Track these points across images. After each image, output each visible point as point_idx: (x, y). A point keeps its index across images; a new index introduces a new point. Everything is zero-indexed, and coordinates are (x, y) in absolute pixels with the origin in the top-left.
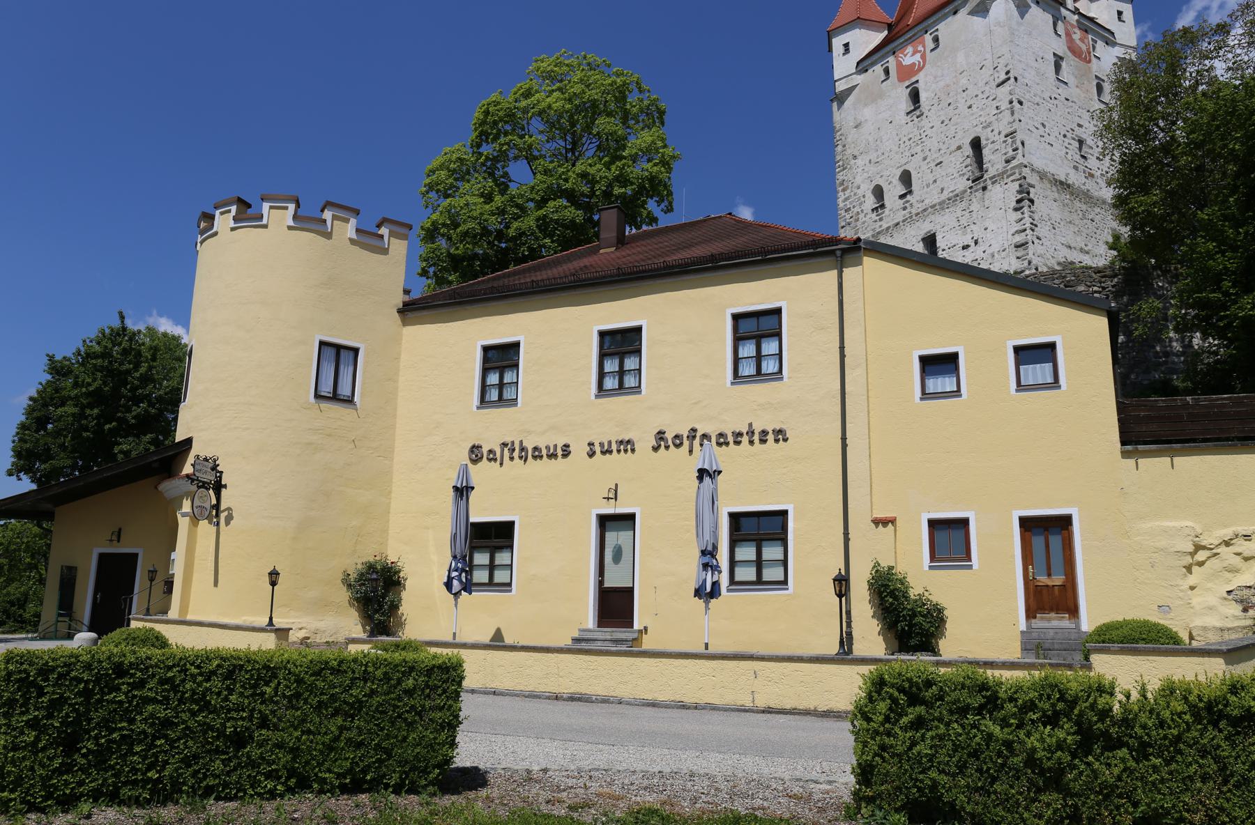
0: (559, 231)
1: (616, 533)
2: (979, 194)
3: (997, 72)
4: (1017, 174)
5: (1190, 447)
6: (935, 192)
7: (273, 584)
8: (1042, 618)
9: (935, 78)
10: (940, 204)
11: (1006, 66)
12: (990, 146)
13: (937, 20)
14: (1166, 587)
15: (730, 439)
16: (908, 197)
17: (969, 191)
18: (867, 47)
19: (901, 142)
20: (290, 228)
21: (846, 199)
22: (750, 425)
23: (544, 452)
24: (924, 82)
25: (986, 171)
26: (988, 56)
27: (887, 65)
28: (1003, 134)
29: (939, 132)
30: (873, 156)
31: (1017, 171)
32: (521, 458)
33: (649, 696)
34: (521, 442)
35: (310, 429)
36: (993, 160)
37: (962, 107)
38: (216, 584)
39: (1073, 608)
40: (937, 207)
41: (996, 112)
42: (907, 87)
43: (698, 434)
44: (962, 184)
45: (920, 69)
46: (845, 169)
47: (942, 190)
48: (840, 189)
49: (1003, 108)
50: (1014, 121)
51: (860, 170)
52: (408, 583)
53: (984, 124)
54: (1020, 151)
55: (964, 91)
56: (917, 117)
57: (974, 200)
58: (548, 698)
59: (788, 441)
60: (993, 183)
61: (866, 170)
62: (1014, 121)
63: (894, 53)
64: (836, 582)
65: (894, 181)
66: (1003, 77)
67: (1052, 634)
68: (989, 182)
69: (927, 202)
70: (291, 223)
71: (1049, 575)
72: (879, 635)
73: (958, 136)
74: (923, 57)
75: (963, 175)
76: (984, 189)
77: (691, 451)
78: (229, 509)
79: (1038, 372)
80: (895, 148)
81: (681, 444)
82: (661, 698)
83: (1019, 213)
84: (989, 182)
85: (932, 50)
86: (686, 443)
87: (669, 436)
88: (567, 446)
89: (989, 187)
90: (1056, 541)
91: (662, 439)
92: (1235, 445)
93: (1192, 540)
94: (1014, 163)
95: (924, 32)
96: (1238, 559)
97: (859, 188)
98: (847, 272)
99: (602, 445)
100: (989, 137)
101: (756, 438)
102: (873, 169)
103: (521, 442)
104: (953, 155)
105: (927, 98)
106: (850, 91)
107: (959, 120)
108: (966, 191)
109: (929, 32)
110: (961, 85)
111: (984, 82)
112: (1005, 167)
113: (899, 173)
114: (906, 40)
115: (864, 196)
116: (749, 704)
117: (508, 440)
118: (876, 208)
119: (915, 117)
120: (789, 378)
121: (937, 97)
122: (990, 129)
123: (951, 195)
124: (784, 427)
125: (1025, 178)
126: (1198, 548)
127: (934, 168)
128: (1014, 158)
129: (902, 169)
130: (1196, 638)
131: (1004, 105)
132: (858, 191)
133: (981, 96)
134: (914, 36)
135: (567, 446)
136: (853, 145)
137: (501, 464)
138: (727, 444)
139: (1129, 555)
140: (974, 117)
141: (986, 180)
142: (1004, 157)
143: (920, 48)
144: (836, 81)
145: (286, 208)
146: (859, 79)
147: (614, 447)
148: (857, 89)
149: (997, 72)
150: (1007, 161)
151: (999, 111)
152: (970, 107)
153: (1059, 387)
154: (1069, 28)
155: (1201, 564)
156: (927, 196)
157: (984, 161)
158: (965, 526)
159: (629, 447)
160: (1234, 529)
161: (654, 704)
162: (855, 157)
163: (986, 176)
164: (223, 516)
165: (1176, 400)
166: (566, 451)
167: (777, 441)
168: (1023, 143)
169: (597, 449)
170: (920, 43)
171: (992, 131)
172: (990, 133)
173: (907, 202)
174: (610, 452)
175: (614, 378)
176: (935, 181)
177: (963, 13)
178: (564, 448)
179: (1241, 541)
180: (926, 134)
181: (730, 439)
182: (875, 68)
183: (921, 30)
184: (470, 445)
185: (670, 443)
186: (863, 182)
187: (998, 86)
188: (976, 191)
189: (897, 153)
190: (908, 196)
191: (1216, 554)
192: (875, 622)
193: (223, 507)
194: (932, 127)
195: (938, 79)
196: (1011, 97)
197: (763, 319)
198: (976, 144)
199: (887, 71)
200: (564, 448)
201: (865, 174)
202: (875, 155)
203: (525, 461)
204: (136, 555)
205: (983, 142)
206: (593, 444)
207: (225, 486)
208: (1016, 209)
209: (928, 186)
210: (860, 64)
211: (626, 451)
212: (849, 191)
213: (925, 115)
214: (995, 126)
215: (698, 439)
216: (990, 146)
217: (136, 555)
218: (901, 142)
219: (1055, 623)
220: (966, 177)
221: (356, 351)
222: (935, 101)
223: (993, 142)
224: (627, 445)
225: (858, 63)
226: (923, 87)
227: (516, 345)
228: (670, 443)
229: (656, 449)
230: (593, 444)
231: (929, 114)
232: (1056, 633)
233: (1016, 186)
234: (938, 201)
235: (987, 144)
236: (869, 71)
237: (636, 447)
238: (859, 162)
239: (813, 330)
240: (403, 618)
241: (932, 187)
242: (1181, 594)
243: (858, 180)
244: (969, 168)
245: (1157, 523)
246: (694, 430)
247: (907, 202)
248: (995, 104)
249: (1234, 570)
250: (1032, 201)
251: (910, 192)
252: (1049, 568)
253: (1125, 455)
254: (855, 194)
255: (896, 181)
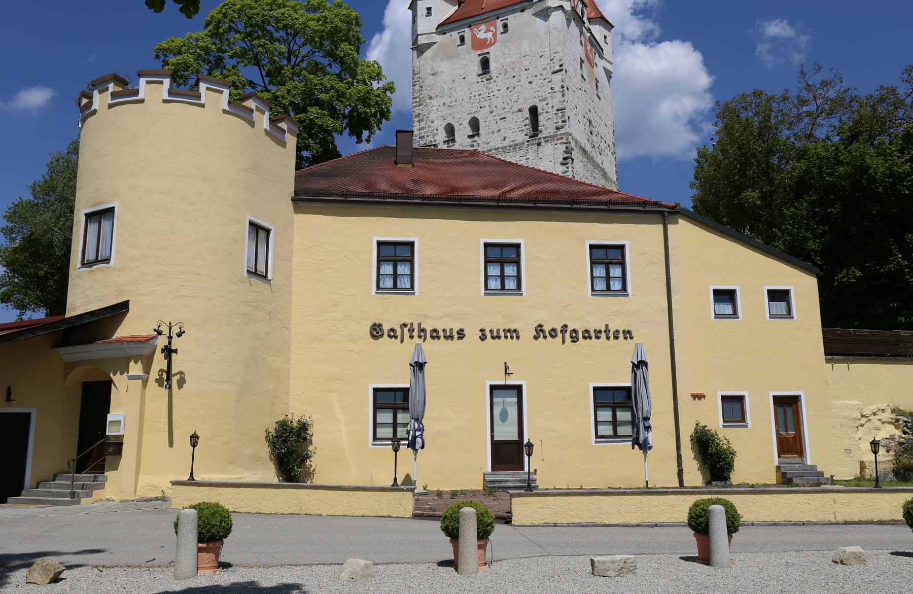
0: (322, 135)
1: (502, 399)
2: (535, 147)
3: (553, 63)
4: (565, 139)
5: (857, 358)
6: (499, 139)
7: (194, 445)
8: (784, 457)
9: (503, 54)
10: (503, 148)
11: (560, 61)
12: (544, 115)
13: (508, 12)
14: (848, 438)
15: (593, 334)
16: (476, 138)
17: (526, 143)
18: (444, 15)
19: (472, 95)
20: (225, 111)
21: (420, 129)
22: (607, 326)
23: (441, 334)
24: (494, 54)
25: (541, 132)
26: (547, 49)
27: (463, 33)
28: (555, 108)
29: (504, 95)
30: (447, 101)
31: (565, 137)
32: (420, 337)
33: (768, 519)
34: (419, 324)
35: (245, 301)
36: (547, 125)
37: (524, 81)
38: (171, 444)
39: (799, 450)
40: (500, 150)
41: (551, 91)
42: (479, 55)
43: (569, 329)
44: (521, 137)
45: (491, 44)
46: (422, 105)
47: (505, 138)
48: (416, 120)
49: (556, 90)
50: (564, 101)
51: (434, 109)
52: (313, 439)
53: (541, 98)
54: (567, 123)
55: (526, 70)
56: (487, 80)
57: (530, 151)
58: (842, 524)
59: (634, 339)
60: (546, 142)
61: (440, 110)
62: (564, 101)
63: (470, 26)
64: (872, 445)
65: (464, 123)
66: (557, 68)
67: (797, 467)
68: (543, 140)
69: (491, 144)
70: (226, 108)
71: (787, 431)
72: (698, 470)
73: (521, 101)
74: (495, 35)
75: (523, 131)
76: (539, 144)
77: (564, 342)
78: (181, 373)
79: (780, 307)
80: (467, 99)
81: (556, 336)
82: (777, 520)
83: (564, 167)
84: (543, 140)
85: (502, 33)
86: (560, 335)
87: (547, 329)
88: (462, 330)
89: (543, 144)
90: (789, 411)
91: (542, 331)
92: (892, 359)
93: (860, 412)
94: (562, 131)
95: (495, 17)
96: (879, 422)
97: (433, 122)
98: (671, 228)
99: (491, 331)
100: (545, 108)
101: (611, 335)
102: (446, 111)
103: (419, 324)
104: (514, 114)
105: (496, 68)
106: (430, 45)
107: (521, 90)
108: (524, 143)
109: (500, 19)
110: (524, 64)
111: (543, 67)
112: (555, 132)
113: (469, 118)
114: (481, 20)
115: (437, 130)
116: (833, 520)
117: (408, 321)
118: (448, 141)
119: (484, 79)
120: (632, 295)
121: (504, 69)
122: (545, 103)
123: (511, 143)
124: (630, 329)
125: (570, 143)
126: (863, 416)
127: (499, 121)
128: (563, 127)
129: (472, 116)
130: (868, 467)
131: (557, 88)
132: (432, 125)
133: (539, 77)
134: (487, 18)
135: (462, 330)
136: (429, 88)
137: (402, 341)
138: (590, 338)
139: (830, 420)
140: (533, 91)
141: (540, 138)
142: (555, 125)
143: (492, 28)
144: (418, 35)
145: (161, 83)
146: (438, 38)
147: (502, 334)
148: (437, 44)
149: (553, 63)
150: (558, 129)
151: (553, 91)
152: (530, 83)
153: (792, 318)
154: (586, 41)
155: (862, 425)
156: (492, 140)
157: (539, 125)
158: (741, 401)
159: (514, 334)
160: (877, 405)
161: (776, 524)
162: (431, 98)
163: (540, 136)
164: (175, 380)
165: (846, 330)
166: (461, 334)
167: (626, 338)
168: (569, 118)
169: (489, 335)
170: (493, 25)
171: (547, 104)
172: (545, 105)
173: (475, 141)
174: (499, 337)
175: (496, 281)
176: (499, 131)
177: (528, 13)
178: (460, 332)
179: (880, 413)
180: (493, 94)
181: (593, 334)
182: (452, 33)
183: (493, 16)
184: (371, 323)
185: (547, 334)
186: (437, 118)
187: (553, 73)
188: (532, 145)
189: (468, 103)
190: (476, 137)
191: (870, 420)
192: (696, 462)
193: (174, 371)
194: (499, 90)
195: (505, 56)
196: (563, 83)
197: (609, 251)
198: (534, 111)
199: (462, 39)
200: (460, 332)
201: (440, 113)
202: (449, 100)
203: (424, 340)
204: (27, 416)
205: (540, 111)
206: (484, 331)
207: (176, 351)
208: (562, 164)
209: (493, 133)
210: (440, 28)
211: (512, 338)
212: (424, 123)
213: (493, 80)
214: (549, 101)
215: (568, 333)
216: (544, 115)
217: (27, 416)
218: (472, 95)
219: (792, 459)
220: (525, 133)
221: (268, 232)
222: (502, 71)
223: (547, 112)
224: (513, 334)
225: (439, 26)
226: (493, 59)
227: (114, 208)
228: (547, 334)
229: (536, 338)
230: (484, 331)
231: (497, 80)
232: (800, 466)
233: (563, 147)
234: (500, 146)
235: (542, 113)
236: (447, 34)
237: (520, 334)
238: (434, 102)
239: (647, 264)
240: (312, 469)
241: (496, 134)
242: (856, 443)
243: (433, 116)
244: (527, 127)
245: (843, 402)
246: (566, 326)
247: (475, 141)
248: (550, 85)
249: (877, 429)
250: (573, 160)
251: (478, 135)
252: (786, 427)
253: (828, 361)
254: (429, 127)
255: (466, 124)
